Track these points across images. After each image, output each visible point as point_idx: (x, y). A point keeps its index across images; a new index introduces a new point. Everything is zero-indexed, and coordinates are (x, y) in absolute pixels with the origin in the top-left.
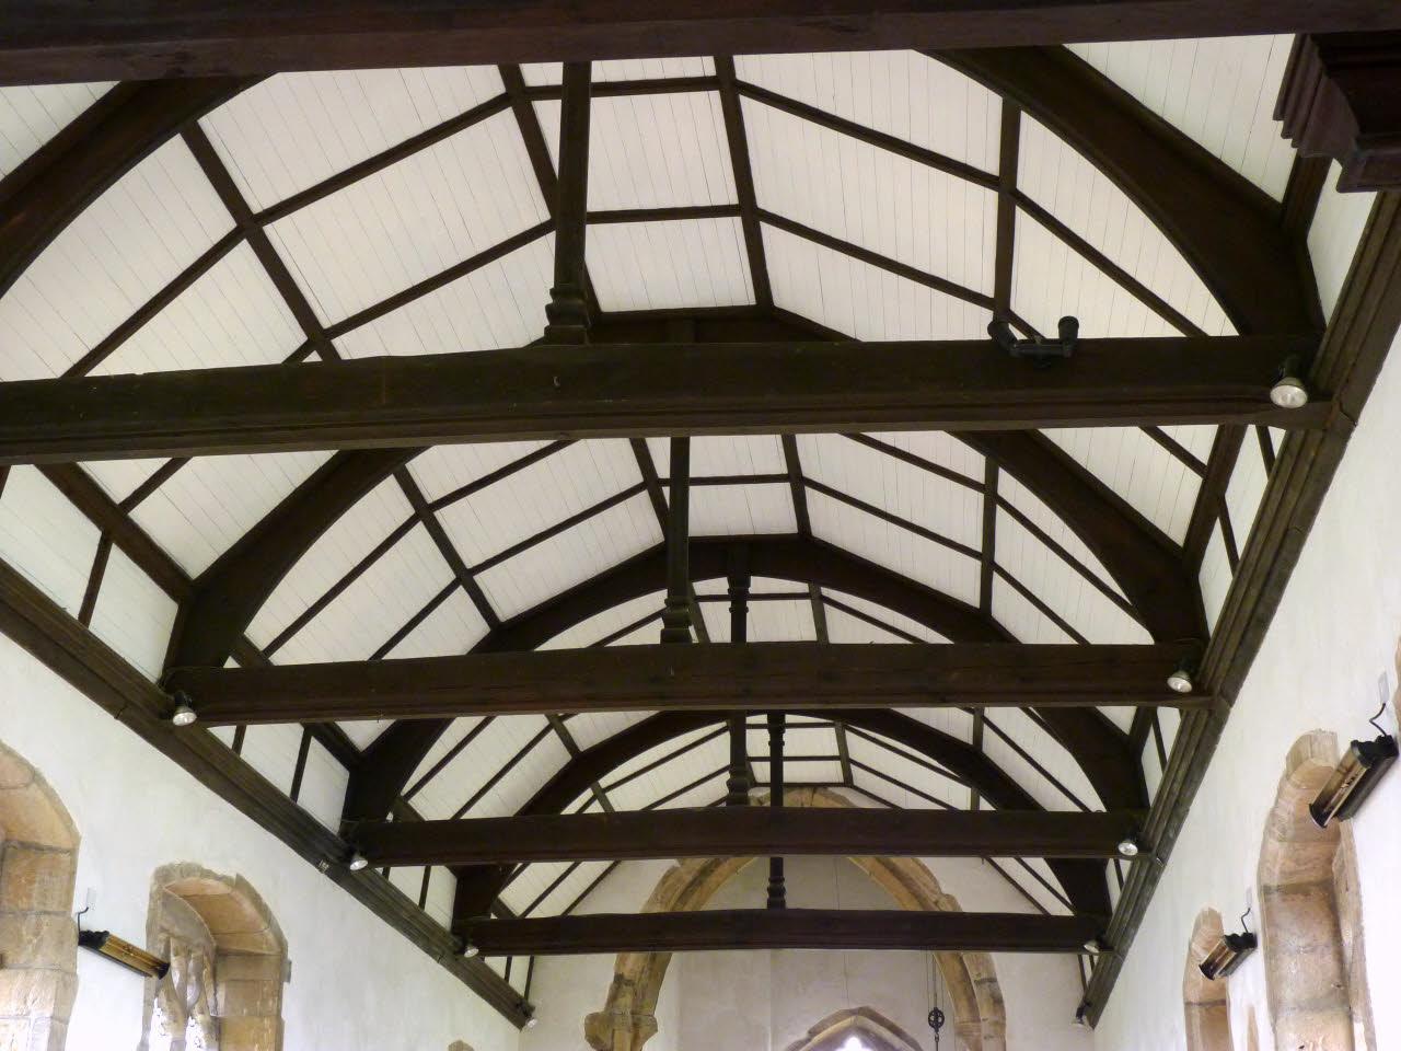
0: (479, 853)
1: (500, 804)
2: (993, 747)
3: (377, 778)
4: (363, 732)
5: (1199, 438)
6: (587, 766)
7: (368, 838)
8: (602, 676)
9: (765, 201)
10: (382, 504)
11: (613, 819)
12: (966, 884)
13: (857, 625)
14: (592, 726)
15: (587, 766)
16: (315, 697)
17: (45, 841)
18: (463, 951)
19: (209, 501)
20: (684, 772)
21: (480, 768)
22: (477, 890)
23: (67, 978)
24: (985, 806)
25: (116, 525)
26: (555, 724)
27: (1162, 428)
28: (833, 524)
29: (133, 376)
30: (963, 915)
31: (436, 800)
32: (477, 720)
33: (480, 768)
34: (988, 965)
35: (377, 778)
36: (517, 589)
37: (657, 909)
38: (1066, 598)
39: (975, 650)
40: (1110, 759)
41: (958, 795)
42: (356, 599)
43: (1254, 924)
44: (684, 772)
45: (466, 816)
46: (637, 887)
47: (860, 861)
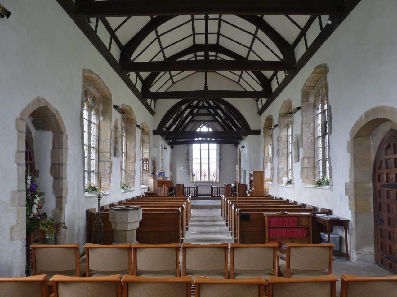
3: (147, 83)
9: (253, 48)
16: (139, 67)
23: (59, 166)
24: (215, 106)
27: (113, 39)
28: (224, 43)
32: (164, 72)
35: (147, 83)
36: (169, 53)
40: (266, 82)
42: (146, 53)
45: (158, 91)
47: (210, 123)
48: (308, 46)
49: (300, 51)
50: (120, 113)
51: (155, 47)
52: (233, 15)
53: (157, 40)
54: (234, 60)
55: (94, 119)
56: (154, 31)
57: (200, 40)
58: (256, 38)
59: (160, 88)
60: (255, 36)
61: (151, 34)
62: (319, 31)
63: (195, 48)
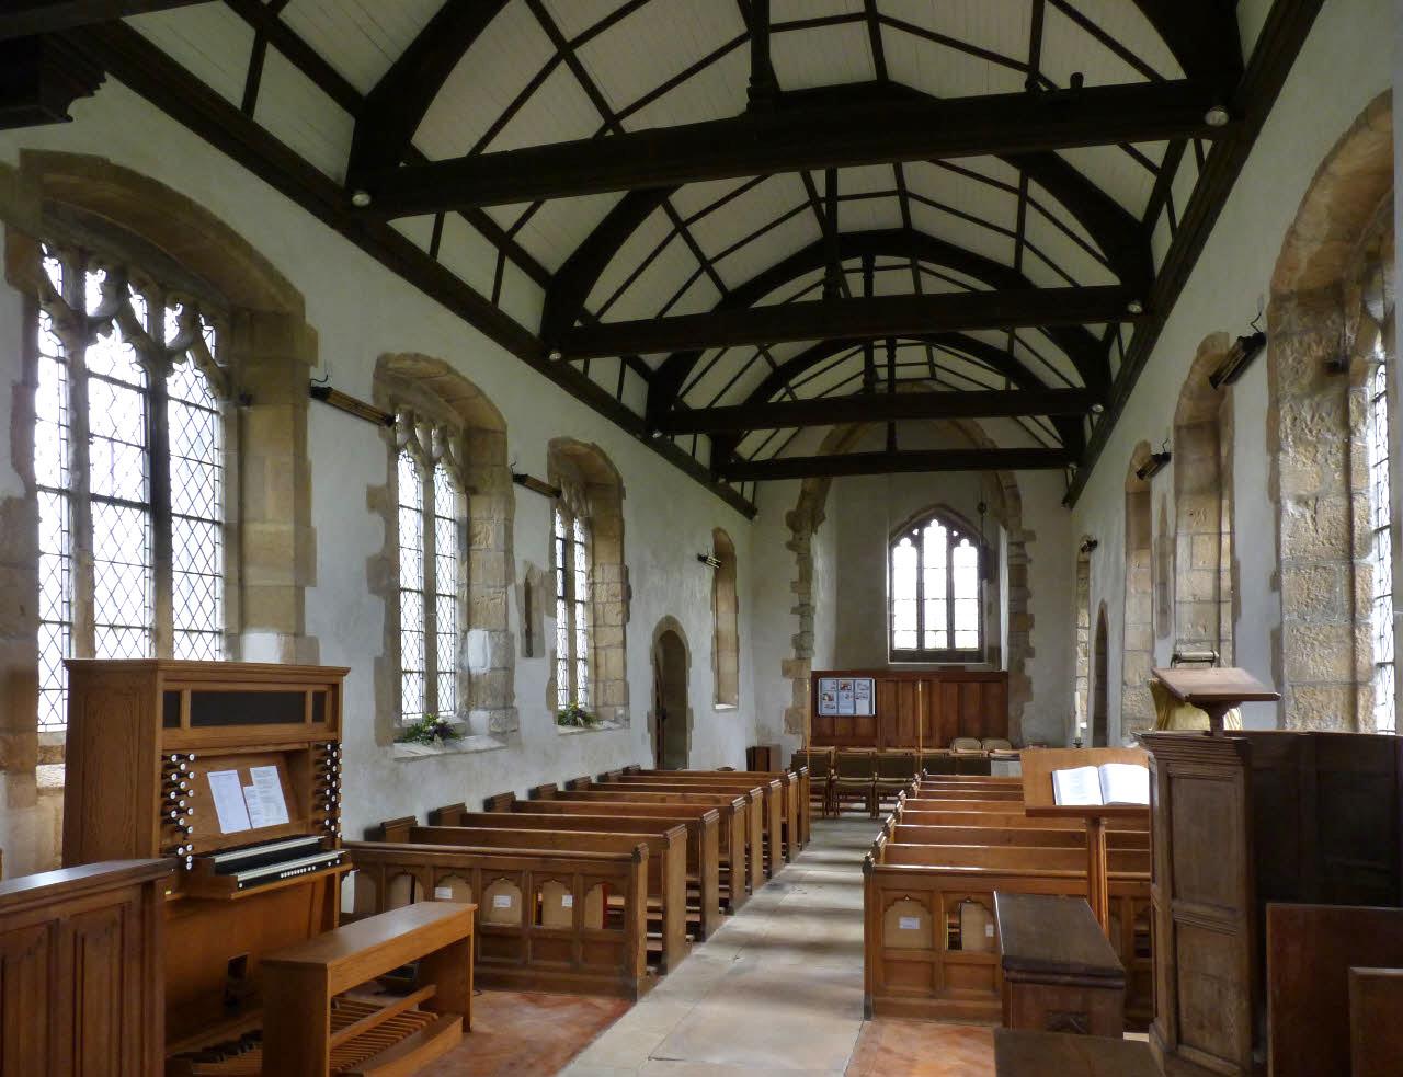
0: (724, 425)
2: (1021, 353)
4: (654, 360)
5: (1156, 150)
6: (782, 375)
7: (661, 420)
8: (789, 320)
10: (655, 224)
12: (1000, 433)
13: (940, 282)
14: (784, 351)
15: (782, 375)
16: (627, 340)
19: (558, 226)
20: (838, 375)
21: (722, 377)
22: (724, 446)
25: (506, 244)
26: (763, 351)
28: (926, 220)
35: (665, 386)
36: (736, 271)
39: (1012, 294)
40: (1090, 356)
41: (998, 382)
42: (645, 283)
43: (1170, 447)
44: (838, 375)
46: (812, 442)
50: (549, 496)
51: (678, 259)
54: (754, 306)
55: (447, 501)
56: (40, 495)
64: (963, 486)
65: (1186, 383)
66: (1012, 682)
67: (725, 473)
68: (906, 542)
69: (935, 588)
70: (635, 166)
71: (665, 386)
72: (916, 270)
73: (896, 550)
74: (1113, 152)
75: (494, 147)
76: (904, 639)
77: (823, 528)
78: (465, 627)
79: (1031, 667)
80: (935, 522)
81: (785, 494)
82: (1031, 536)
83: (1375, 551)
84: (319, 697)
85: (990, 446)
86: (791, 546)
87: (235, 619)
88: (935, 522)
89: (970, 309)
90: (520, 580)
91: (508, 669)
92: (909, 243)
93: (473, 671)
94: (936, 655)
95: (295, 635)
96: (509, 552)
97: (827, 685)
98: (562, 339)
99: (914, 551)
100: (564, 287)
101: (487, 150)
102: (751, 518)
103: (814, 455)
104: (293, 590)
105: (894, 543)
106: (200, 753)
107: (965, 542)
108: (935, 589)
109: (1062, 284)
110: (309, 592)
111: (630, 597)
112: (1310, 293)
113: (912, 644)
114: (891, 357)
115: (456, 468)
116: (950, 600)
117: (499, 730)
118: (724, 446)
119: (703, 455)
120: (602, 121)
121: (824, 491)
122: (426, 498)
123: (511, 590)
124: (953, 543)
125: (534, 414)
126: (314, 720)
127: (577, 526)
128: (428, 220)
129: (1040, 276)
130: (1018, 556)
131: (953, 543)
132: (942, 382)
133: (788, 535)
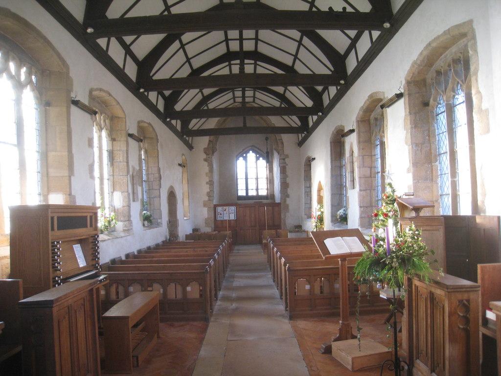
0: (185, 117)
1: (190, 107)
2: (288, 95)
4: (167, 93)
5: (352, 33)
6: (206, 99)
7: (167, 115)
8: (213, 81)
10: (176, 45)
11: (208, 110)
12: (276, 121)
13: (264, 69)
14: (207, 91)
15: (206, 99)
17: (120, 116)
18: (183, 136)
19: (145, 44)
20: (223, 101)
21: (188, 100)
22: (185, 124)
25: (127, 48)
26: (201, 91)
28: (263, 49)
29: (146, 16)
30: (276, 127)
31: (178, 107)
33: (188, 100)
34: (281, 137)
35: (170, 102)
36: (197, 63)
37: (217, 127)
38: (320, 66)
39: (290, 76)
40: (317, 97)
41: (276, 103)
42: (170, 67)
43: (355, 127)
44: (223, 101)
46: (212, 123)
48: (360, 59)
49: (351, 64)
51: (180, 58)
52: (269, 30)
53: (181, 50)
57: (234, 46)
58: (301, 46)
59: (177, 72)
60: (300, 43)
61: (176, 41)
62: (369, 45)
63: (229, 57)
64: (258, 139)
65: (362, 107)
66: (282, 206)
67: (186, 135)
68: (241, 159)
69: (252, 175)
70: (172, 26)
71: (170, 102)
72: (256, 65)
73: (238, 161)
74: (338, 33)
75: (128, 16)
76: (242, 193)
77: (215, 154)
78: (112, 191)
79: (288, 201)
80: (251, 152)
81: (203, 142)
82: (287, 156)
83: (438, 161)
84: (91, 217)
85: (273, 126)
86: (205, 160)
87: (46, 189)
88: (251, 152)
89: (273, 79)
90: (131, 173)
91: (129, 206)
92: (256, 56)
93: (116, 208)
94: (252, 198)
95: (69, 195)
96: (127, 162)
97: (219, 209)
98: (142, 84)
99: (244, 162)
100: (146, 65)
101: (127, 16)
102: (191, 150)
103: (213, 127)
104: (68, 177)
105: (237, 159)
106: (63, 240)
107: (261, 159)
108: (253, 174)
109: (309, 72)
110: (72, 178)
111: (161, 179)
112: (417, 82)
113: (244, 194)
114: (244, 94)
115: (108, 131)
116: (247, 179)
117: (126, 229)
118: (185, 124)
119: (179, 128)
120: (164, 8)
121: (217, 141)
122: (101, 140)
123: (129, 176)
124: (257, 159)
125: (133, 111)
126: (58, 230)
127: (142, 152)
128: (106, 39)
129: (300, 69)
130: (283, 163)
131: (257, 159)
132: (257, 104)
133: (205, 156)
